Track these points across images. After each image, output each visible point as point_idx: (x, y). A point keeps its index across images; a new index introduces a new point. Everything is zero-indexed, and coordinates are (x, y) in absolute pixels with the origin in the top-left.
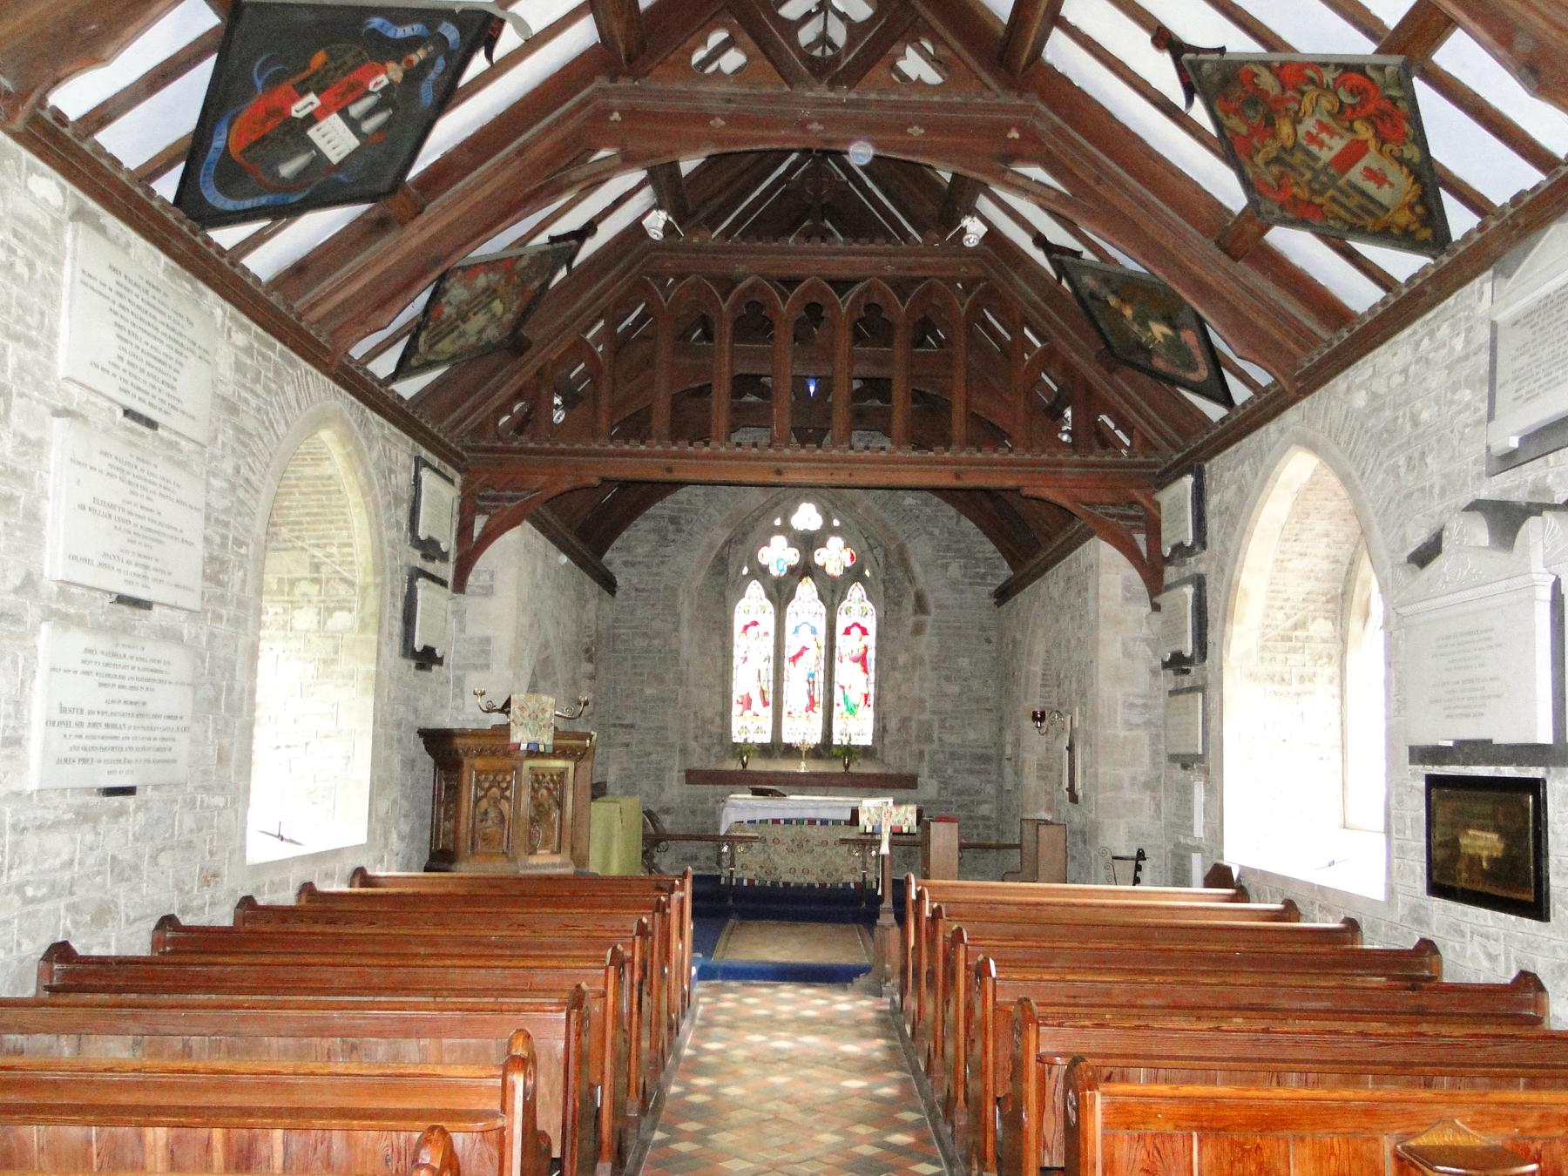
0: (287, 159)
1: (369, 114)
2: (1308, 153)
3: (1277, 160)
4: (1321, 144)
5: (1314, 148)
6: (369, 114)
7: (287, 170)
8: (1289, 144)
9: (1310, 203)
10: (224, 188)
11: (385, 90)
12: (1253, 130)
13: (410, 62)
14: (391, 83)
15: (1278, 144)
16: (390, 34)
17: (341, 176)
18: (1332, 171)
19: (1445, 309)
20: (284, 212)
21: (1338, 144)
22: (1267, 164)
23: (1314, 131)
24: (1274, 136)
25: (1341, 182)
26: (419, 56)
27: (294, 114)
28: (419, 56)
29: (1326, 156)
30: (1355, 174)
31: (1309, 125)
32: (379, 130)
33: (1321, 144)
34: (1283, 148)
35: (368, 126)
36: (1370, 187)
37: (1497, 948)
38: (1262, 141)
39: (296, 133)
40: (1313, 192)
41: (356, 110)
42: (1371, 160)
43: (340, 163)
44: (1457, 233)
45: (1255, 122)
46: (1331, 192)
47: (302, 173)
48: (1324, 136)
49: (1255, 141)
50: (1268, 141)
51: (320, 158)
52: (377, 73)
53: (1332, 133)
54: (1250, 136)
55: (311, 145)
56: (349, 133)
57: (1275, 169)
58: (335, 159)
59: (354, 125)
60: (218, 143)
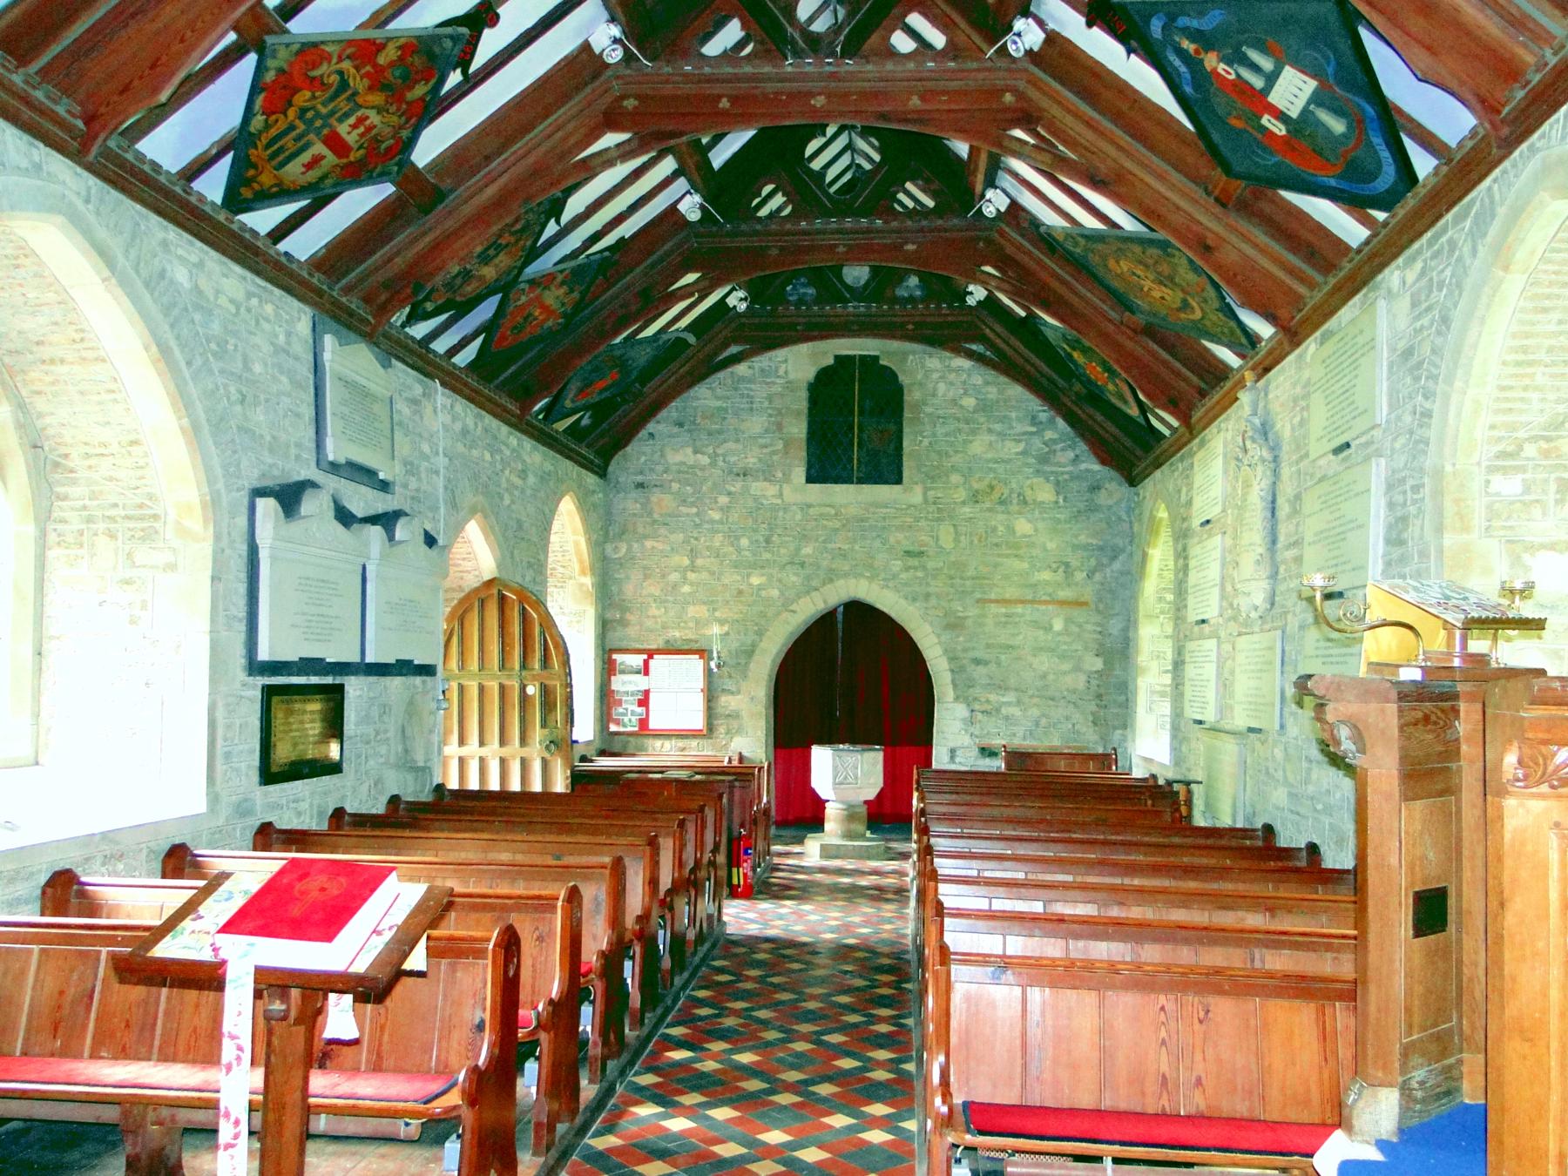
0: (1328, 130)
1: (1256, 68)
2: (347, 115)
3: (344, 85)
4: (354, 127)
5: (352, 120)
6: (1256, 68)
7: (1338, 126)
8: (360, 100)
9: (291, 105)
10: (1372, 176)
11: (1230, 64)
12: (379, 70)
13: (1197, 52)
14: (1221, 60)
15: (360, 88)
16: (1188, 76)
17: (1330, 70)
18: (325, 131)
19: (272, 292)
20: (1391, 121)
21: (352, 138)
22: (341, 73)
23: (368, 122)
24: (371, 88)
25: (312, 136)
26: (1188, 46)
27: (1284, 132)
28: (1188, 46)
29: (343, 129)
30: (319, 148)
31: (374, 118)
32: (1264, 49)
33: (354, 127)
34: (355, 94)
35: (1267, 64)
36: (306, 157)
37: (304, 806)
38: (367, 75)
39: (1301, 126)
40: (303, 111)
41: (1258, 83)
42: (331, 159)
43: (1313, 77)
44: (247, 218)
45: (388, 74)
46: (302, 127)
47: (1338, 112)
48: (362, 129)
49: (368, 68)
50: (366, 82)
51: (1316, 99)
52: (1219, 75)
53: (362, 135)
54: (375, 65)
55: (1305, 112)
56: (1280, 81)
57: (335, 78)
58: (1312, 84)
59: (1272, 79)
60: (1333, 182)
